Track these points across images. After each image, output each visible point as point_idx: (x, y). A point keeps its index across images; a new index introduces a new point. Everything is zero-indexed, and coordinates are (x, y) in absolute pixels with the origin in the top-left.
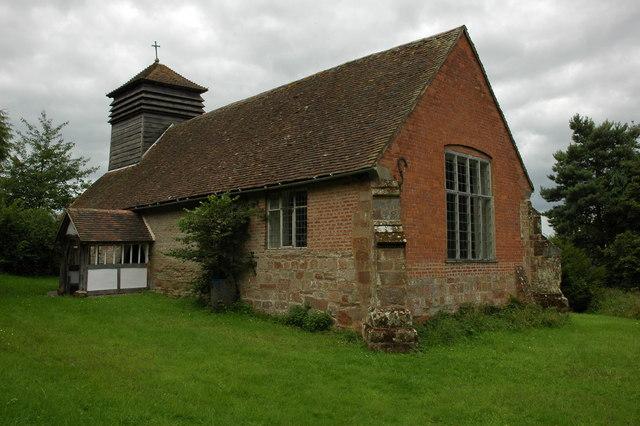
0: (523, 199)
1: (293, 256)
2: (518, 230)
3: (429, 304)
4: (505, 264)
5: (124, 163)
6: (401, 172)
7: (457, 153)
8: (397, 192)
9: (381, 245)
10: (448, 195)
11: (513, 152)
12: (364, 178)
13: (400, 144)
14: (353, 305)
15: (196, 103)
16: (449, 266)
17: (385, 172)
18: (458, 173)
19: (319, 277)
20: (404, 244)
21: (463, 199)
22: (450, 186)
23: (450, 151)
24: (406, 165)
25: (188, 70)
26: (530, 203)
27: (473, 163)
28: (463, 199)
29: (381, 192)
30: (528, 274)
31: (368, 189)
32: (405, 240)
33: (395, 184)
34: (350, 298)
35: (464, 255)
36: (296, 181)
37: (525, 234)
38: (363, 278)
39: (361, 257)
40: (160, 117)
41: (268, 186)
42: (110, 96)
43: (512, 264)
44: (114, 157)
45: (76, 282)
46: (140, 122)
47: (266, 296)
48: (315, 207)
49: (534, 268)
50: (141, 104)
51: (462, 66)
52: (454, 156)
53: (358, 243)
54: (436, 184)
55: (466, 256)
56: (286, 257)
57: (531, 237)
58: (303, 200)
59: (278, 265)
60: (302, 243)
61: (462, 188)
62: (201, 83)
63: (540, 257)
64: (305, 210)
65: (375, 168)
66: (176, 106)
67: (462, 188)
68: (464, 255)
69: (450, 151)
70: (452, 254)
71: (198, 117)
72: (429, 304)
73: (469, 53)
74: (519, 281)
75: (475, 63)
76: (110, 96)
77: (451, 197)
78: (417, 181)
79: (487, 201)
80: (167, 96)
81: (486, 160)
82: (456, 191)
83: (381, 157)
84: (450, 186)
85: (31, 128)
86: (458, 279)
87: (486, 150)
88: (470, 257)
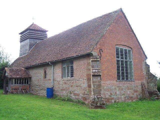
0: (143, 61)
1: (70, 80)
2: (142, 70)
3: (111, 94)
4: (137, 82)
5: (24, 54)
6: (101, 53)
7: (120, 47)
8: (99, 60)
9: (94, 76)
10: (117, 60)
11: (139, 46)
12: (89, 55)
13: (100, 45)
14: (87, 94)
15: (45, 35)
16: (118, 82)
17: (95, 53)
18: (120, 53)
19: (77, 86)
20: (100, 75)
21: (126, 62)
22: (118, 57)
23: (117, 46)
24: (102, 51)
25: (42, 25)
26: (146, 62)
27: (126, 50)
28: (122, 61)
29: (94, 59)
30: (146, 85)
31: (90, 59)
32: (101, 74)
33: (98, 57)
34: (86, 93)
35: (123, 79)
36: (69, 57)
37: (145, 73)
38: (89, 86)
39: (89, 79)
40: (34, 40)
41: (62, 59)
42: (20, 34)
43: (140, 82)
44: (23, 43)
45: (8, 90)
46: (28, 41)
47: (62, 93)
48: (76, 65)
49: (148, 83)
50: (28, 36)
51: (121, 20)
52: (119, 48)
53: (88, 75)
54: (113, 57)
55: (128, 79)
56: (67, 80)
57: (147, 73)
58: (72, 63)
59: (65, 83)
60: (72, 76)
61: (122, 58)
62: (46, 29)
63: (150, 79)
64: (73, 66)
65: (92, 52)
66: (39, 36)
67: (126, 58)
68: (127, 79)
69: (117, 46)
70: (119, 79)
71: (45, 39)
72: (111, 94)
73: (123, 16)
74: (142, 87)
75: (125, 19)
76: (20, 34)
77: (118, 61)
78: (106, 56)
79: (131, 62)
80: (36, 33)
81: (130, 49)
82: (124, 60)
83: (93, 49)
84: (118, 57)
85: (51, 94)
86: (121, 87)
87: (130, 46)
88: (125, 79)
